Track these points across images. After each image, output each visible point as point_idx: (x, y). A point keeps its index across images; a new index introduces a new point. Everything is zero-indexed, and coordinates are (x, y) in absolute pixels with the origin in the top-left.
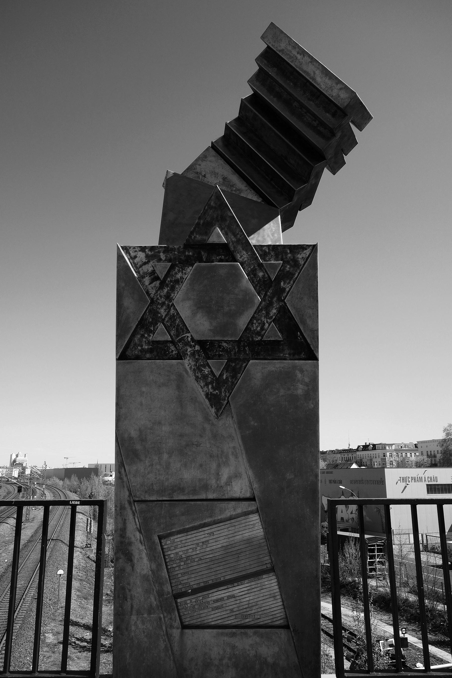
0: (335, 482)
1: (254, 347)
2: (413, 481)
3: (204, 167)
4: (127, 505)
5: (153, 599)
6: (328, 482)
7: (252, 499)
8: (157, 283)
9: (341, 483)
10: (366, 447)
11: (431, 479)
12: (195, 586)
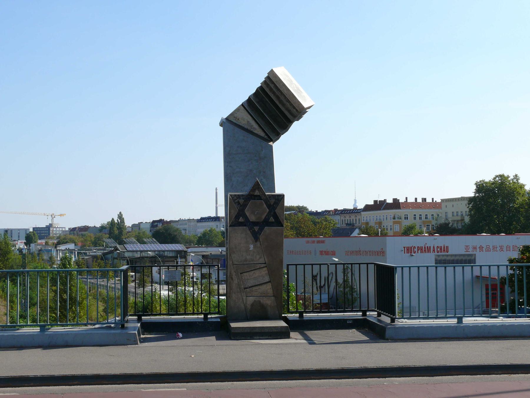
0: (327, 253)
1: (266, 223)
2: (419, 251)
3: (238, 115)
6: (318, 253)
7: (265, 263)
8: (239, 205)
9: (334, 254)
10: (379, 205)
11: (441, 249)
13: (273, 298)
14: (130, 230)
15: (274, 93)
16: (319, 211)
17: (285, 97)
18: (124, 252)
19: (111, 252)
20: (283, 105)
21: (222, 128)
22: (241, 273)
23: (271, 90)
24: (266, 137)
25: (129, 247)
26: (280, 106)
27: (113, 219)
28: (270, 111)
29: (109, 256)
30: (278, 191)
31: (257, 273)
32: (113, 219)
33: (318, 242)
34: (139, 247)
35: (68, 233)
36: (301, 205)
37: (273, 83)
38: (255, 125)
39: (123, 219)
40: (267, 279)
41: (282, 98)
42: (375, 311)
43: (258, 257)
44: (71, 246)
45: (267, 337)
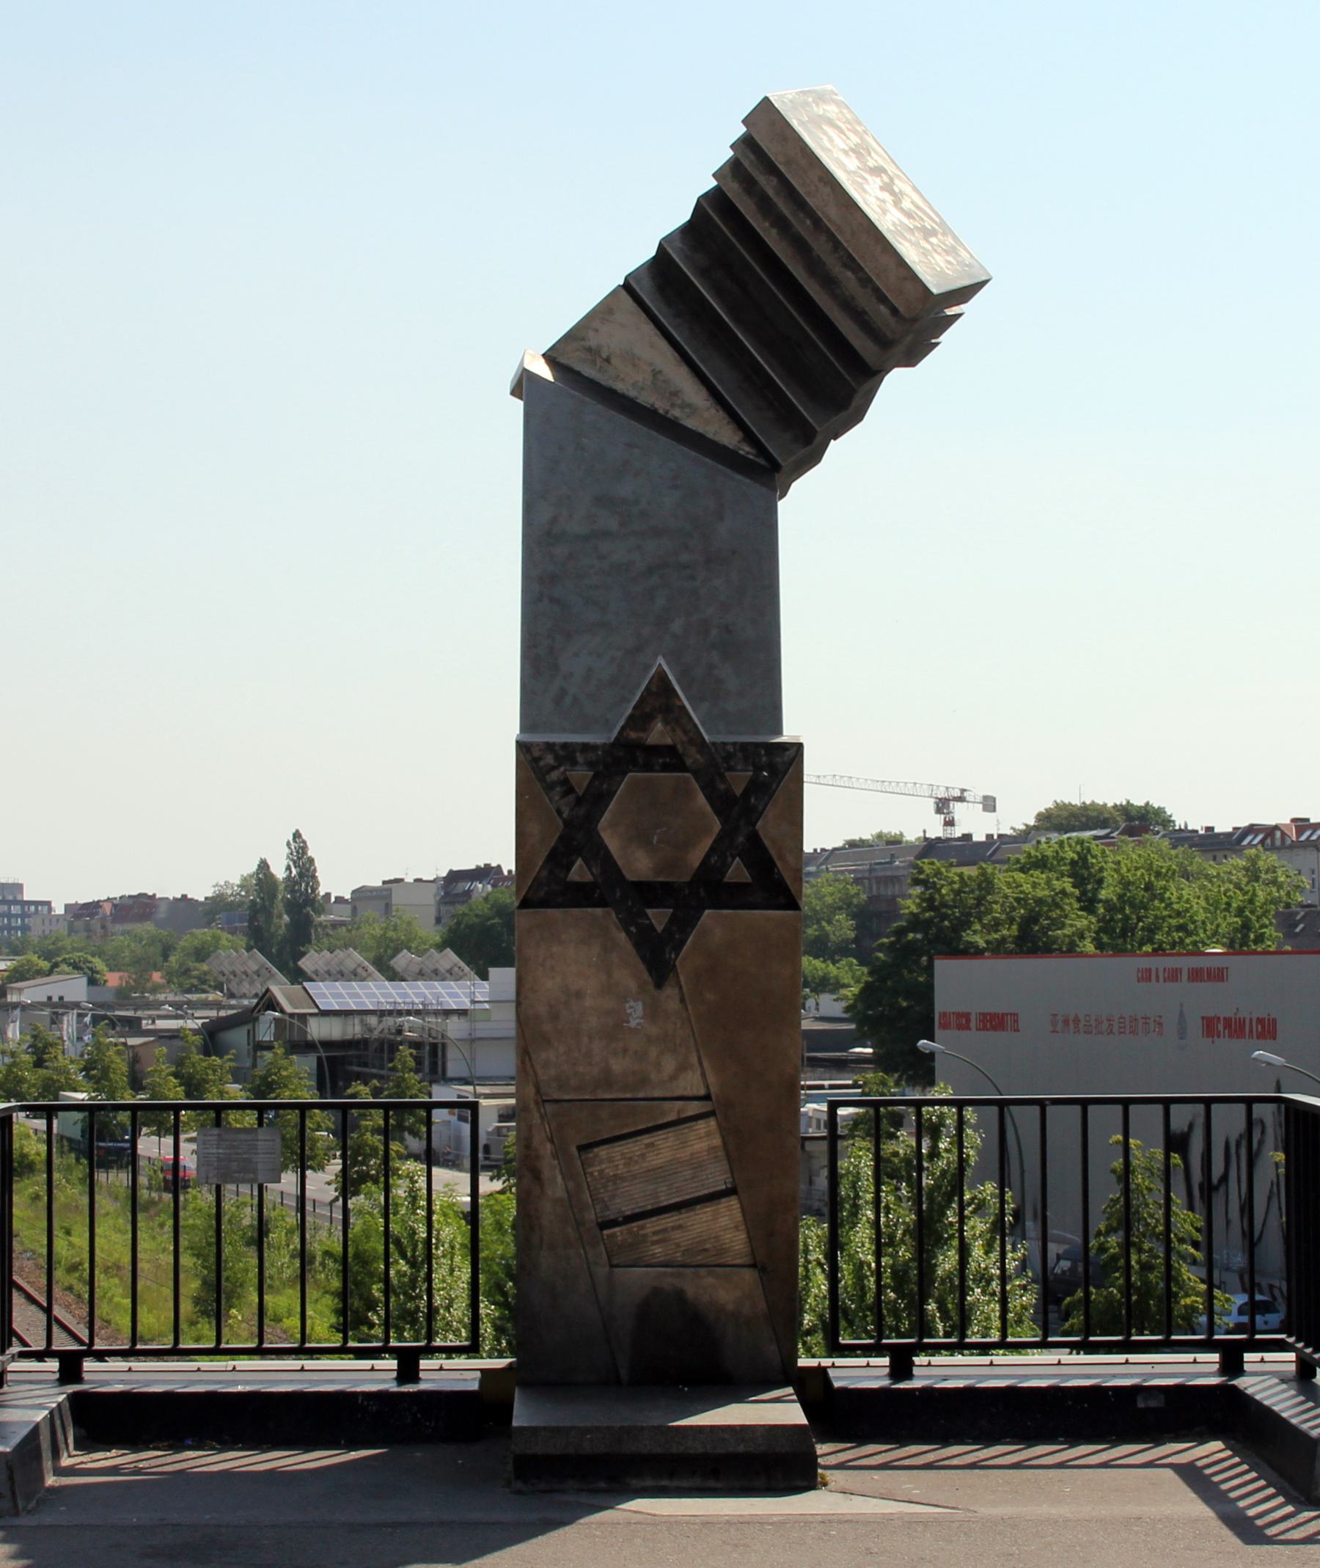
0: (1236, 1028)
1: (710, 889)
4: (533, 1106)
5: (570, 1230)
6: (1195, 1027)
7: (707, 1097)
8: (571, 798)
12: (628, 1213)
13: (749, 1276)
14: (343, 914)
15: (782, 224)
16: (1223, 827)
17: (837, 245)
18: (303, 1017)
19: (247, 1018)
20: (829, 282)
21: (519, 404)
22: (583, 1148)
23: (765, 205)
24: (746, 450)
25: (329, 994)
26: (813, 289)
27: (264, 865)
28: (772, 312)
29: (238, 1037)
30: (790, 732)
31: (664, 1148)
32: (264, 865)
33: (1196, 975)
34: (374, 993)
35: (63, 929)
36: (1138, 802)
37: (771, 169)
38: (693, 393)
39: (311, 861)
40: (717, 1177)
41: (820, 247)
42: (1280, 1346)
43: (669, 1065)
44: (74, 988)
45: (697, 1482)
